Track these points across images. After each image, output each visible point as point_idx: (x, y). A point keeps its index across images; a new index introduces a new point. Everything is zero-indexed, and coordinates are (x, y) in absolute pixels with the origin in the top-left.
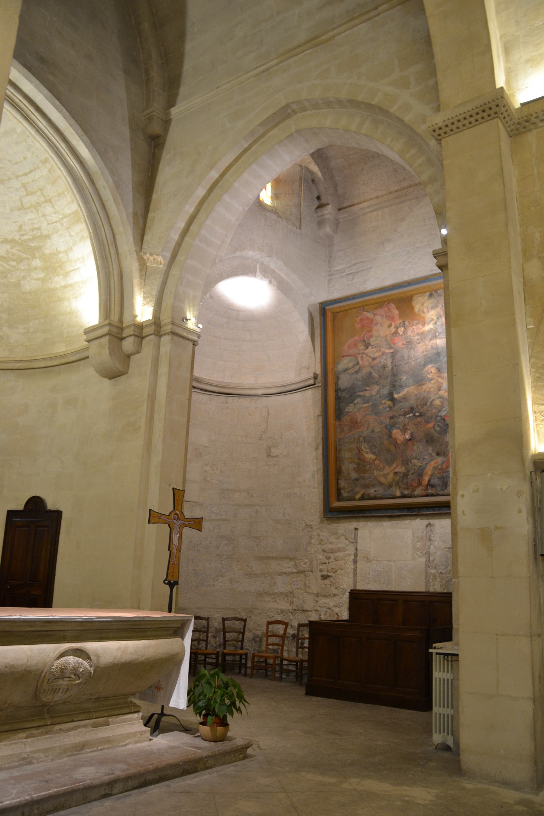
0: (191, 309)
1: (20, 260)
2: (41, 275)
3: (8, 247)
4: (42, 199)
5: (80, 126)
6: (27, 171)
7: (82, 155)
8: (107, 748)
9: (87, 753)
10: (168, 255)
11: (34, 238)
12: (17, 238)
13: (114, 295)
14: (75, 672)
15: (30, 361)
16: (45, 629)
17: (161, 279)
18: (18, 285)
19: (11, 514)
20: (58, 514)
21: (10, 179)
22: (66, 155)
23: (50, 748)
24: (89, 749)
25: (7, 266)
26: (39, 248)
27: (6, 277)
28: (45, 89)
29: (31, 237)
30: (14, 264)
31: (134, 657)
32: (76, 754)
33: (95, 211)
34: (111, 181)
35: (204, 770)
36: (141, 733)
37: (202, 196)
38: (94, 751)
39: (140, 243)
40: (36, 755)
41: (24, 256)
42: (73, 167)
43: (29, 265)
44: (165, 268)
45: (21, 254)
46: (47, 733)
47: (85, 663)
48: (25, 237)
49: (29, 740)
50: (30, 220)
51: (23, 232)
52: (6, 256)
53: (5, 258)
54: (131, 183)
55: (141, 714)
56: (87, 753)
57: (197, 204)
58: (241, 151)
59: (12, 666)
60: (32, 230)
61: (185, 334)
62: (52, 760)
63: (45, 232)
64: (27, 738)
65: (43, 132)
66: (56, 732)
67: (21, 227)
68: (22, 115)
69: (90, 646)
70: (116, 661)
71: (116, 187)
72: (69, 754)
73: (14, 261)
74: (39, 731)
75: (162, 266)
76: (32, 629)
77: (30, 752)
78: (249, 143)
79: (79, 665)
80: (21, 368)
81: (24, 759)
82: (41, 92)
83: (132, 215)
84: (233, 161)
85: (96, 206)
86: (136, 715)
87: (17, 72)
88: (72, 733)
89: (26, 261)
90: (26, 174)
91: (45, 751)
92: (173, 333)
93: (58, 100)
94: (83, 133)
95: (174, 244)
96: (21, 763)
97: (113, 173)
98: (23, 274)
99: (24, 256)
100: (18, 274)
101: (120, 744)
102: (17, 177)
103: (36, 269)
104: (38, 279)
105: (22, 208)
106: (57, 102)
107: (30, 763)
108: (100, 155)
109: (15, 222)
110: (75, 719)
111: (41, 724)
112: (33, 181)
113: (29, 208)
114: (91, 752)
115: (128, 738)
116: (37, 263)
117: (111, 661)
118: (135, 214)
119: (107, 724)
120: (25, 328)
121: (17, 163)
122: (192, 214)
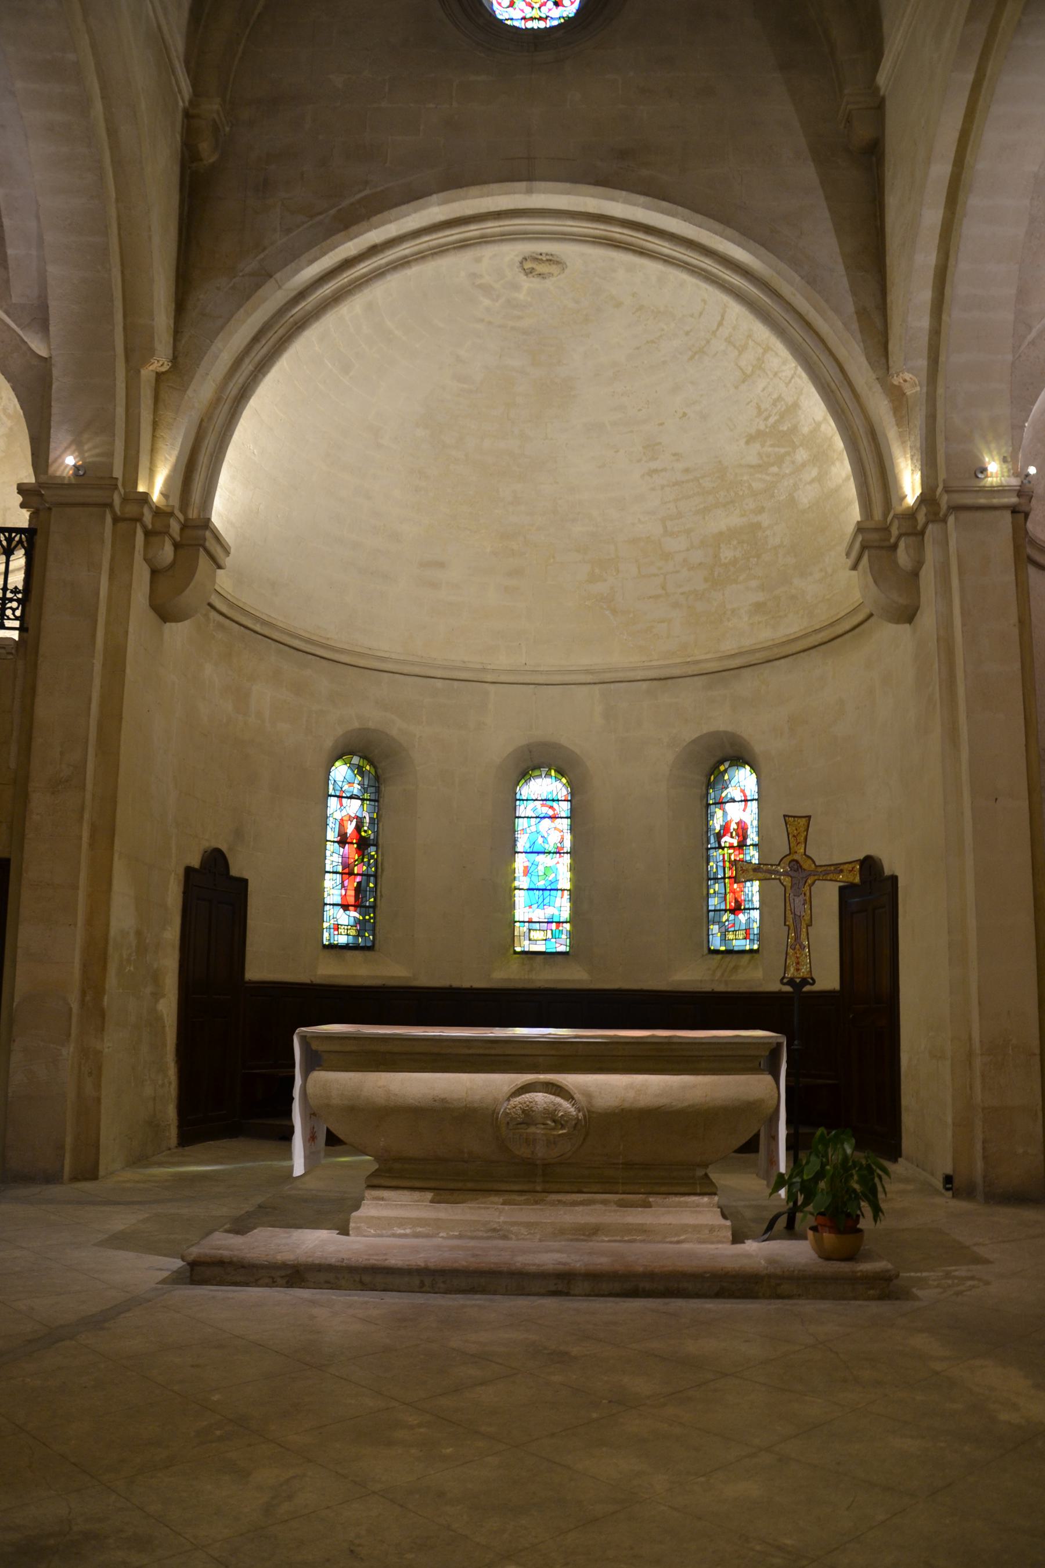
0: (993, 445)
1: (780, 460)
2: (814, 472)
3: (758, 446)
4: (761, 351)
5: (714, 219)
6: (719, 318)
7: (741, 259)
8: (641, 1241)
9: (603, 1241)
10: (922, 363)
11: (782, 416)
12: (762, 427)
13: (874, 473)
14: (551, 1115)
15: (832, 625)
16: (493, 1052)
17: (924, 413)
18: (792, 501)
19: (189, 871)
20: (894, 879)
21: (708, 342)
22: (720, 274)
23: (537, 1224)
24: (606, 1236)
25: (768, 478)
26: (794, 429)
27: (772, 496)
28: (638, 196)
29: (776, 418)
30: (774, 469)
31: (662, 1101)
32: (583, 1240)
33: (801, 340)
34: (798, 279)
35: (771, 1297)
36: (712, 1229)
37: (940, 223)
38: (615, 1241)
39: (883, 361)
40: (514, 1229)
41: (782, 450)
42: (740, 288)
43: (793, 462)
44: (925, 390)
45: (777, 449)
46: (536, 1203)
47: (566, 1105)
48: (772, 420)
49: (506, 1207)
50: (764, 390)
51: (765, 414)
52: (760, 462)
53: (760, 466)
54: (840, 260)
55: (716, 1198)
56: (603, 1241)
57: (937, 241)
58: (967, 93)
59: (443, 1100)
60: (774, 404)
61: (982, 501)
62: (540, 1240)
63: (790, 400)
64: (503, 1204)
65: (674, 258)
66: (553, 1204)
67: (759, 408)
68: (635, 252)
69: (571, 1080)
70: (626, 1105)
71: (808, 283)
72: (570, 1237)
73: (773, 465)
74: (523, 1198)
75: (918, 388)
76: (471, 1052)
77: (505, 1223)
78: (973, 67)
79: (557, 1107)
80: (825, 640)
81: (494, 1230)
82: (635, 205)
83: (855, 316)
84: (964, 122)
85: (797, 332)
86: (706, 1199)
87: (591, 199)
88: (580, 1208)
89: (788, 458)
90: (720, 324)
91: (528, 1225)
92: (957, 508)
93: (664, 200)
94: (722, 226)
95: (927, 338)
96: (489, 1234)
97: (794, 263)
98: (791, 481)
99: (782, 450)
100: (786, 484)
101: (668, 1240)
102: (714, 333)
103: (804, 465)
104: (812, 481)
105: (746, 378)
106: (665, 204)
107: (505, 1237)
108: (763, 245)
109: (748, 404)
110: (585, 1190)
111: (525, 1187)
112: (734, 328)
113: (753, 372)
114: (609, 1241)
115: (689, 1230)
116: (802, 455)
117: (617, 1104)
118: (862, 314)
119: (647, 1205)
120: (821, 570)
121: (701, 313)
122: (936, 266)
